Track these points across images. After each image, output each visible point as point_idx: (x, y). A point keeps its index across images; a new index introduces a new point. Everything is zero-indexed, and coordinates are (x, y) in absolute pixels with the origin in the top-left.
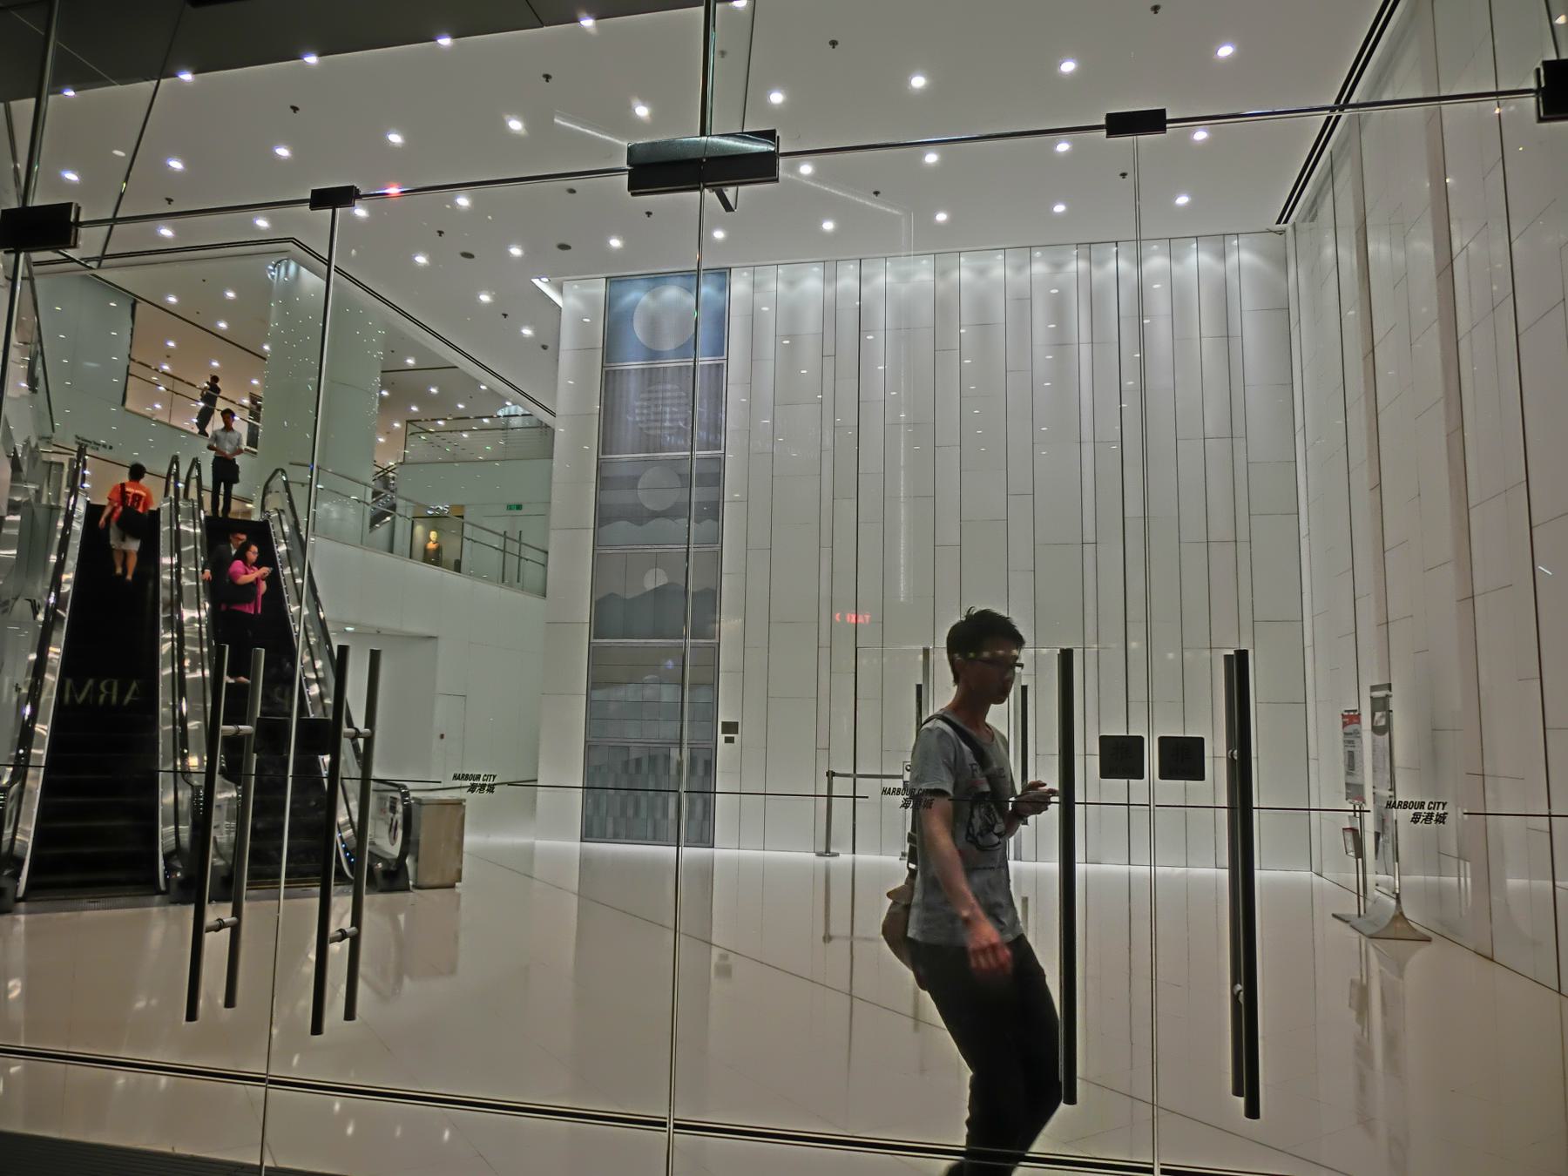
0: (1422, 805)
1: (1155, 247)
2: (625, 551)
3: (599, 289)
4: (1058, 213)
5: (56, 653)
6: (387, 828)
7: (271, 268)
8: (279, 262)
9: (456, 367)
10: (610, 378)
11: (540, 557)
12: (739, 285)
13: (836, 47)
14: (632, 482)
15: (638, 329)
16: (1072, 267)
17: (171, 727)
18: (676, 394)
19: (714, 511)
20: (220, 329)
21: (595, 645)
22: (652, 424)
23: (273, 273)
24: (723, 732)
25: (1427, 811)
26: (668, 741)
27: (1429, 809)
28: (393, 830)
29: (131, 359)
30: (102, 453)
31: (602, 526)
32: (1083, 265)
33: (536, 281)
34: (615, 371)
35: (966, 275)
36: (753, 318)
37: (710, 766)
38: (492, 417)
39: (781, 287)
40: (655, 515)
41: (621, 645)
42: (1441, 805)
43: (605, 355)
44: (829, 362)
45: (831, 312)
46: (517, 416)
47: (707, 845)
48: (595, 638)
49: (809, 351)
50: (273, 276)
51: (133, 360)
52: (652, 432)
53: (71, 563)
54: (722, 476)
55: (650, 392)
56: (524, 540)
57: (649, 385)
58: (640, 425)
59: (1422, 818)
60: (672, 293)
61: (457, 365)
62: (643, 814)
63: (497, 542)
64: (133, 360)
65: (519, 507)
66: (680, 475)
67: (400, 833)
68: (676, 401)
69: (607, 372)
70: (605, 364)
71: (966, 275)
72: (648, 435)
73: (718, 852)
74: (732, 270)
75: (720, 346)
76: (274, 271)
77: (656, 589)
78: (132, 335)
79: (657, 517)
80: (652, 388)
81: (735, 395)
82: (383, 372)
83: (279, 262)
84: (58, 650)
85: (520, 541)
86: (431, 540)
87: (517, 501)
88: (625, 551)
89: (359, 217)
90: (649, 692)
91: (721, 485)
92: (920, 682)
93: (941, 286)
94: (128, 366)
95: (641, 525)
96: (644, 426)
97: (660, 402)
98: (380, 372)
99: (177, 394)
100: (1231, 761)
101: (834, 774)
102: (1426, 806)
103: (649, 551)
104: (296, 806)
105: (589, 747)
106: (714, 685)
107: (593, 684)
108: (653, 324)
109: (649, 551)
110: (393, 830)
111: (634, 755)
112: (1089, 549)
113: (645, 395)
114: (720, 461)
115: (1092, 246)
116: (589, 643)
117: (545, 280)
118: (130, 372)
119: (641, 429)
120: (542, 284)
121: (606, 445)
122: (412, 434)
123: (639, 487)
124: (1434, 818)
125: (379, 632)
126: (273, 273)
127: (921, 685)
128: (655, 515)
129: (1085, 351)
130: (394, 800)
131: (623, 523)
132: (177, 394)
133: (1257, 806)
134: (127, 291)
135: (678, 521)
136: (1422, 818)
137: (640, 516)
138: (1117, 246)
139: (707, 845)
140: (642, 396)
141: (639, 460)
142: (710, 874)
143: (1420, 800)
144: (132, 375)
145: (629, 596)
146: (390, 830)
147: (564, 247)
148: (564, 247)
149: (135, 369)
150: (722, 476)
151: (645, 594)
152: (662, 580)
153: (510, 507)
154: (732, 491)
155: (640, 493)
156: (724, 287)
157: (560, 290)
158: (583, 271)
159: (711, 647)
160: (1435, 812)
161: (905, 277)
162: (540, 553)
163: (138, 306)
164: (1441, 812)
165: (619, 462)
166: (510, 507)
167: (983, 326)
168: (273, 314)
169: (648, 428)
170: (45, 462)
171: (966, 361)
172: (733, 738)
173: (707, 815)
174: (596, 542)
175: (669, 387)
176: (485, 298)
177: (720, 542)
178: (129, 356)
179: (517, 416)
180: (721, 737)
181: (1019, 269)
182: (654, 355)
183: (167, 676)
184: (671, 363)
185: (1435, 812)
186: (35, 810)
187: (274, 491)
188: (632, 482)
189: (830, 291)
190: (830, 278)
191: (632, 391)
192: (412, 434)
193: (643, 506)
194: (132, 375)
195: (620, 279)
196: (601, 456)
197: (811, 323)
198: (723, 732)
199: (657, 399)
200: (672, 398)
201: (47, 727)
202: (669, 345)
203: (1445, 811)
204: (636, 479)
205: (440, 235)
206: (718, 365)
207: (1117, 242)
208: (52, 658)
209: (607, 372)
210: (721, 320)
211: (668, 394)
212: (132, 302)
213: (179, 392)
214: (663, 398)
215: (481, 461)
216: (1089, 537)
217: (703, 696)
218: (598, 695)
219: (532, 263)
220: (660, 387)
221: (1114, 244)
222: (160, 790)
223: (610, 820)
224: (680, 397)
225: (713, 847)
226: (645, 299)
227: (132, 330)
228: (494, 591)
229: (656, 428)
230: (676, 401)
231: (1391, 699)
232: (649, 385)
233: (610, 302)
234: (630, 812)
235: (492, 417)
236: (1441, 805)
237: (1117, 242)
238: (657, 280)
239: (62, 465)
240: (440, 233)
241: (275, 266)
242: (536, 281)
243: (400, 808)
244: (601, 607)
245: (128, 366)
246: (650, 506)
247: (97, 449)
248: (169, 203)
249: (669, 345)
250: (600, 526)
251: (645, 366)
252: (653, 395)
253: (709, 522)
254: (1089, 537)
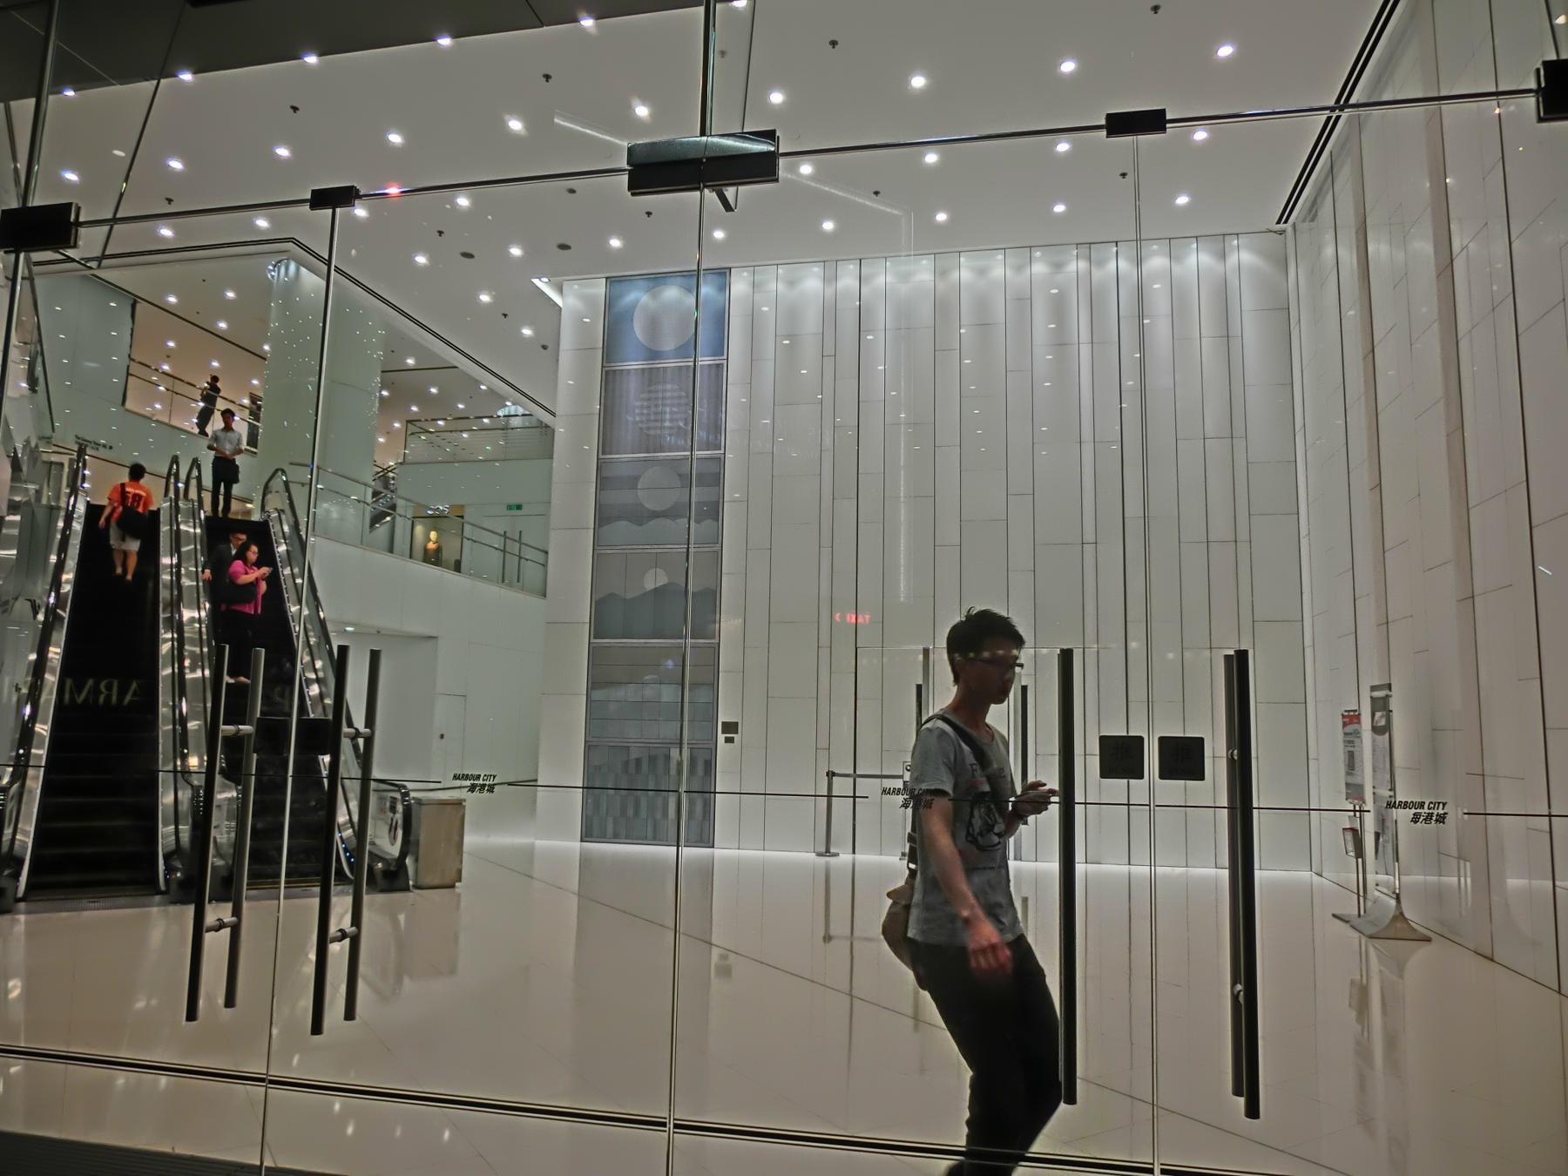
0: (1422, 805)
1: (1155, 247)
2: (625, 551)
3: (599, 289)
4: (1058, 213)
5: (56, 653)
6: (387, 828)
7: (271, 268)
8: (279, 262)
9: (456, 367)
10: (610, 378)
11: (540, 557)
12: (739, 285)
13: (836, 47)
14: (632, 482)
15: (638, 329)
16: (1072, 267)
17: (171, 727)
18: (676, 394)
19: (714, 511)
20: (220, 329)
21: (595, 645)
22: (652, 424)
23: (273, 273)
24: (723, 732)
25: (1427, 811)
26: (668, 741)
27: (1429, 809)
28: (393, 830)
29: (131, 359)
30: (102, 453)
31: (602, 526)
32: (1083, 265)
33: (536, 281)
34: (615, 371)
35: (966, 275)
36: (753, 318)
37: (710, 766)
38: (492, 417)
39: (781, 287)
40: (655, 515)
41: (621, 645)
42: (1441, 805)
43: (605, 355)
44: (829, 362)
45: (831, 312)
46: (517, 416)
47: (707, 845)
48: (595, 638)
49: (809, 351)
50: (273, 276)
51: (133, 360)
52: (652, 432)
53: (71, 563)
54: (722, 476)
55: (650, 392)
56: (524, 540)
57: (649, 385)
58: (640, 425)
59: (1422, 818)
60: (672, 293)
61: (457, 365)
62: (643, 814)
63: (497, 542)
64: (133, 360)
65: (519, 507)
66: (680, 475)
67: (400, 833)
68: (676, 401)
69: (607, 372)
70: (605, 364)
71: (966, 275)
72: (648, 435)
73: (718, 852)
74: (732, 270)
75: (720, 346)
76: (274, 271)
77: (656, 589)
78: (132, 335)
79: (657, 517)
80: (652, 388)
81: (735, 395)
82: (383, 372)
83: (279, 262)
84: (58, 650)
85: (520, 541)
86: (431, 540)
87: (517, 501)
88: (625, 551)
89: (359, 217)
90: (649, 692)
91: (721, 485)
92: (920, 682)
93: (941, 286)
94: (128, 366)
95: (641, 525)
96: (644, 426)
97: (660, 402)
98: (380, 372)
99: (177, 394)
100: (1231, 761)
101: (834, 774)
102: (1426, 806)
103: (649, 551)
105: (589, 747)
106: (714, 685)
107: (593, 684)
108: (653, 324)
109: (649, 551)
110: (393, 830)
111: (634, 755)
112: (1089, 549)
113: (645, 395)
114: (720, 461)
115: (1092, 246)
116: (589, 643)
117: (545, 280)
118: (130, 372)
119: (641, 429)
120: (542, 284)
121: (606, 445)
122: (412, 434)
123: (639, 487)
124: (1434, 818)
125: (379, 632)
126: (273, 273)
127: (921, 685)
128: (655, 515)
129: (1085, 351)
130: (394, 800)
131: (623, 523)
132: (177, 394)
133: (1257, 806)
134: (127, 291)
135: (678, 521)
136: (1422, 818)
137: (640, 516)
138: (1117, 246)
139: (707, 845)
140: (642, 396)
141: (639, 460)
142: (710, 874)
143: (1420, 800)
144: (132, 375)
145: (629, 596)
146: (390, 830)
147: (564, 247)
148: (564, 247)
149: (135, 369)
150: (722, 476)
151: (645, 594)
152: (662, 580)
153: (510, 507)
154: (732, 491)
155: (640, 493)
156: (724, 287)
157: (560, 290)
158: (583, 271)
159: (711, 647)
160: (1435, 812)
161: (905, 277)
162: (540, 553)
163: (138, 306)
164: (1441, 812)
165: (619, 462)
166: (510, 507)
167: (983, 326)
168: (273, 314)
169: (648, 428)
170: (45, 462)
171: (966, 361)
172: (733, 738)
173: (707, 815)
174: (596, 542)
175: (669, 387)
176: (485, 298)
177: (720, 542)
178: (129, 356)
179: (517, 416)
180: (721, 737)
181: (1019, 269)
182: (654, 355)
183: (167, 676)
184: (671, 363)
185: (1435, 812)
186: (35, 810)
187: (274, 491)
188: (632, 482)
189: (830, 291)
190: (830, 278)
191: (632, 391)
192: (412, 434)
193: (643, 506)
194: (132, 375)
195: (620, 279)
196: (601, 456)
197: (811, 323)
198: (723, 732)
199: (657, 399)
200: (672, 398)
201: (47, 727)
202: (669, 345)
203: (1445, 811)
204: (636, 479)
205: (440, 235)
206: (718, 365)
207: (1117, 242)
208: (52, 658)
209: (607, 372)
210: (721, 320)
211: (668, 394)
212: (132, 302)
213: (179, 392)
214: (663, 398)
215: (481, 461)
216: (1089, 537)
217: (703, 696)
218: (598, 695)
219: (532, 263)
220: (660, 387)
221: (1114, 244)
222: (160, 790)
223: (610, 820)
224: (680, 397)
225: (713, 847)
226: (645, 299)
227: (132, 330)
228: (494, 591)
229: (656, 428)
230: (676, 401)
231: (1391, 699)
232: (649, 385)
233: (610, 302)
234: (630, 812)
235: (492, 417)
236: (1441, 805)
237: (1117, 242)
238: (657, 280)
239: (62, 465)
240: (440, 233)
241: (275, 266)
242: (536, 281)
243: (400, 808)
244: (601, 607)
245: (128, 366)
246: (650, 506)
247: (97, 449)
248: (169, 203)
249: (669, 345)
250: (600, 526)
251: (645, 366)
252: (653, 395)
253: (709, 522)
254: (1089, 537)
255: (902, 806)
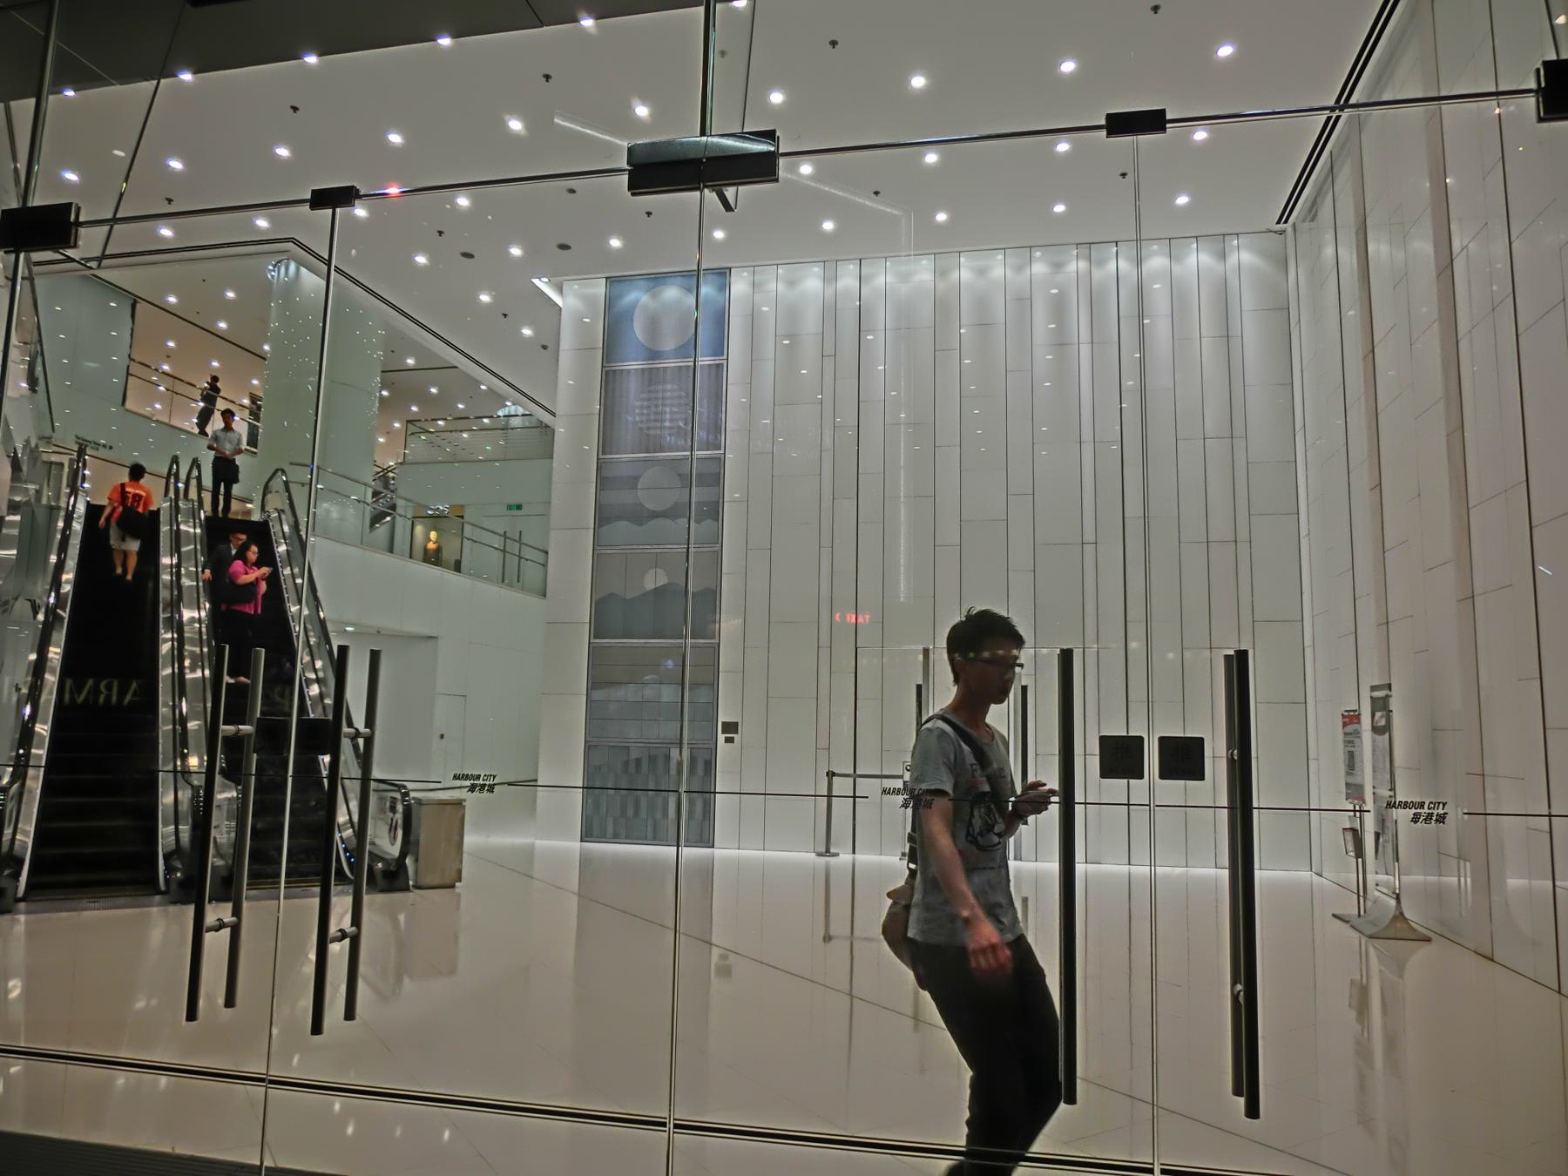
0: (1422, 805)
1: (1155, 247)
2: (625, 551)
3: (599, 289)
4: (1058, 213)
5: (56, 653)
6: (387, 828)
7: (271, 268)
8: (279, 262)
9: (456, 367)
10: (610, 378)
11: (540, 557)
12: (739, 285)
13: (836, 47)
14: (632, 482)
15: (638, 329)
16: (1072, 267)
17: (171, 727)
18: (676, 394)
19: (714, 511)
20: (220, 329)
21: (595, 645)
22: (652, 424)
23: (273, 273)
24: (723, 732)
25: (1427, 811)
26: (668, 741)
27: (1429, 809)
28: (393, 830)
29: (131, 359)
30: (102, 453)
31: (602, 526)
32: (1083, 265)
33: (536, 281)
34: (615, 371)
35: (966, 275)
36: (753, 318)
37: (710, 766)
38: (492, 417)
39: (781, 287)
40: (655, 515)
41: (621, 645)
42: (1441, 805)
43: (605, 355)
44: (829, 362)
45: (831, 312)
46: (517, 416)
47: (707, 845)
48: (595, 638)
49: (809, 351)
50: (273, 276)
51: (133, 360)
52: (652, 432)
53: (71, 563)
54: (722, 476)
55: (650, 392)
56: (524, 540)
57: (649, 385)
58: (640, 425)
59: (1422, 818)
60: (672, 293)
61: (457, 365)
62: (643, 814)
63: (497, 542)
64: (133, 360)
65: (519, 507)
66: (680, 475)
67: (400, 833)
68: (676, 401)
69: (607, 372)
70: (605, 364)
71: (966, 275)
72: (648, 435)
73: (718, 852)
74: (732, 270)
75: (720, 346)
76: (274, 271)
77: (656, 589)
78: (132, 335)
79: (657, 517)
80: (652, 388)
81: (735, 395)
82: (383, 372)
83: (279, 262)
84: (58, 650)
85: (520, 541)
86: (431, 540)
87: (517, 501)
88: (625, 551)
89: (359, 217)
90: (649, 692)
91: (721, 485)
92: (920, 682)
93: (941, 286)
94: (128, 366)
95: (641, 525)
96: (644, 426)
97: (660, 402)
98: (380, 372)
99: (177, 394)
100: (1231, 761)
101: (834, 774)
102: (1426, 806)
103: (649, 551)
104: (296, 806)
105: (589, 747)
106: (714, 685)
107: (593, 684)
108: (653, 324)
109: (649, 551)
110: (393, 830)
111: (634, 755)
112: (1089, 549)
113: (645, 395)
114: (720, 461)
115: (1092, 246)
116: (589, 643)
117: (545, 280)
118: (130, 372)
119: (641, 429)
120: (542, 284)
121: (606, 445)
122: (412, 434)
123: (639, 487)
124: (1434, 818)
125: (379, 632)
126: (273, 273)
127: (921, 685)
128: (655, 515)
129: (1085, 351)
130: (394, 800)
131: (623, 523)
132: (177, 394)
133: (1257, 806)
134: (127, 291)
135: (678, 521)
136: (1422, 818)
137: (640, 516)
138: (1117, 246)
139: (707, 845)
140: (642, 396)
141: (639, 460)
142: (710, 874)
143: (1420, 800)
144: (132, 375)
145: (629, 596)
146: (390, 830)
147: (564, 247)
148: (564, 247)
149: (135, 369)
150: (722, 476)
151: (645, 594)
152: (662, 580)
153: (510, 507)
154: (732, 491)
155: (640, 493)
156: (724, 287)
157: (560, 290)
158: (583, 271)
159: (711, 647)
160: (1435, 812)
161: (905, 277)
162: (540, 553)
163: (138, 306)
164: (1441, 812)
165: (619, 462)
166: (510, 507)
167: (983, 326)
168: (273, 314)
169: (648, 428)
170: (45, 462)
171: (966, 361)
172: (733, 738)
173: (707, 815)
174: (596, 542)
175: (669, 387)
176: (485, 298)
177: (720, 542)
178: (129, 356)
179: (517, 416)
180: (721, 737)
181: (1019, 269)
182: (654, 355)
183: (167, 676)
184: (671, 363)
185: (1435, 812)
187: (274, 491)
188: (632, 482)
189: (830, 291)
190: (830, 278)
191: (632, 391)
192: (412, 434)
193: (643, 506)
194: (132, 375)
195: (620, 279)
196: (601, 456)
197: (811, 323)
198: (723, 732)
199: (657, 399)
200: (672, 398)
201: (47, 727)
202: (669, 345)
203: (1445, 811)
204: (636, 479)
205: (440, 235)
206: (718, 365)
207: (1117, 242)
208: (52, 658)
209: (607, 372)
210: (721, 320)
211: (668, 394)
212: (132, 302)
213: (179, 392)
214: (663, 398)
215: (481, 461)
216: (1089, 537)
217: (703, 696)
218: (598, 695)
219: (532, 263)
220: (660, 387)
221: (1114, 244)
222: (160, 790)
223: (610, 820)
224: (680, 397)
225: (713, 847)
226: (645, 299)
227: (132, 330)
228: (494, 591)
229: (656, 428)
230: (676, 401)
231: (1391, 699)
232: (649, 385)
233: (610, 302)
234: (630, 812)
235: (492, 417)
236: (1441, 805)
237: (1117, 242)
238: (657, 280)
239: (62, 465)
240: (440, 233)
241: (275, 266)
242: (536, 281)
244: (601, 607)
245: (128, 366)
246: (650, 506)
247: (97, 449)
248: (169, 203)
249: (669, 345)
250: (600, 526)
251: (645, 366)
252: (653, 395)
253: (709, 522)
254: (1089, 537)
255: (902, 806)
